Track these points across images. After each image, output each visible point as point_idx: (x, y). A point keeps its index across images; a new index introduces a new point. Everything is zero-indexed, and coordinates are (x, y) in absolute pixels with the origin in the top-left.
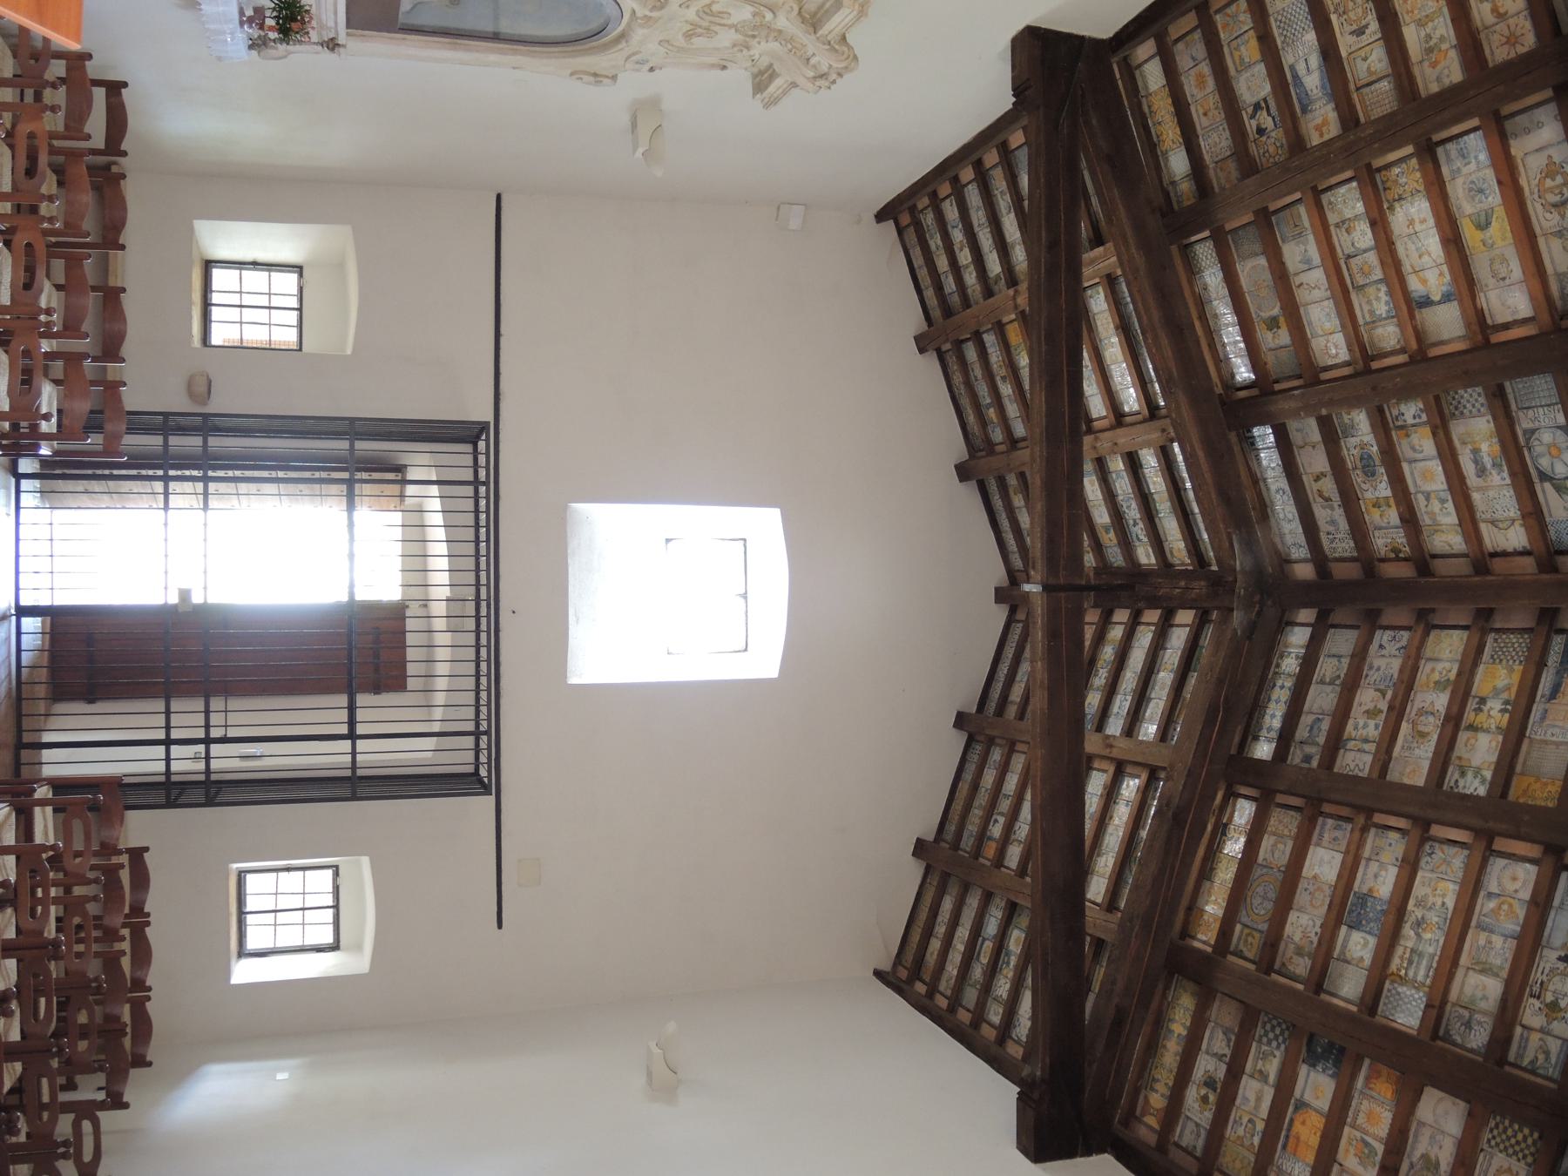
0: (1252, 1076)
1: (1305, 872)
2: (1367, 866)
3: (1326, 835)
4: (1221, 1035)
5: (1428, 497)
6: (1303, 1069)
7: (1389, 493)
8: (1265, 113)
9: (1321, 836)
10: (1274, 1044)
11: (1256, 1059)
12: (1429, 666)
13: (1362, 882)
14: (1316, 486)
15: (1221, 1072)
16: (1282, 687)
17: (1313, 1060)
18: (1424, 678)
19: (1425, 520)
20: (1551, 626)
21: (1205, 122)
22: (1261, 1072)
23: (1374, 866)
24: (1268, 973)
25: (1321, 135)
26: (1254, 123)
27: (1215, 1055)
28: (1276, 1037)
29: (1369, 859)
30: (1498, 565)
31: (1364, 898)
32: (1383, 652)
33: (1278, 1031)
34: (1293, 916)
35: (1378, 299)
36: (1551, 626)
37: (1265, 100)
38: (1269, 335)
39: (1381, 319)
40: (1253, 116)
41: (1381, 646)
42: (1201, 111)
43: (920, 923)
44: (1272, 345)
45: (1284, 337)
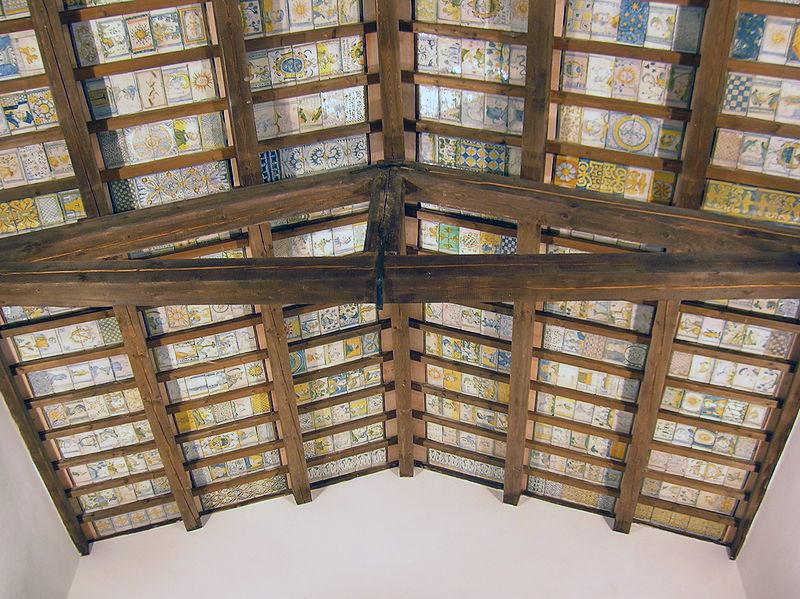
0: (775, 112)
1: (607, 95)
2: (596, 34)
3: (575, 81)
4: (747, 153)
5: (316, 14)
6: (763, 58)
7: (313, 48)
8: (14, 111)
9: (578, 85)
10: (746, 93)
11: (761, 110)
12: (442, 15)
13: (609, 35)
14: (310, 122)
15: (777, 143)
16: (466, 155)
17: (754, 49)
18: (451, 17)
19: (333, 21)
20: (422, 355)
21: (18, 175)
22: (771, 104)
23: (596, 27)
24: (682, 162)
25: (35, 57)
26: (22, 124)
27: (764, 156)
28: (741, 92)
29: (591, 33)
30: (368, 18)
31: (621, 26)
32: (434, 61)
33: (735, 92)
34: (644, 99)
35: (164, 28)
36: (422, 355)
37: (6, 109)
38: (189, 143)
39: (179, 28)
40: (17, 124)
41: (430, 65)
42: (9, 178)
43: (684, 520)
44: (198, 141)
45: (190, 125)
